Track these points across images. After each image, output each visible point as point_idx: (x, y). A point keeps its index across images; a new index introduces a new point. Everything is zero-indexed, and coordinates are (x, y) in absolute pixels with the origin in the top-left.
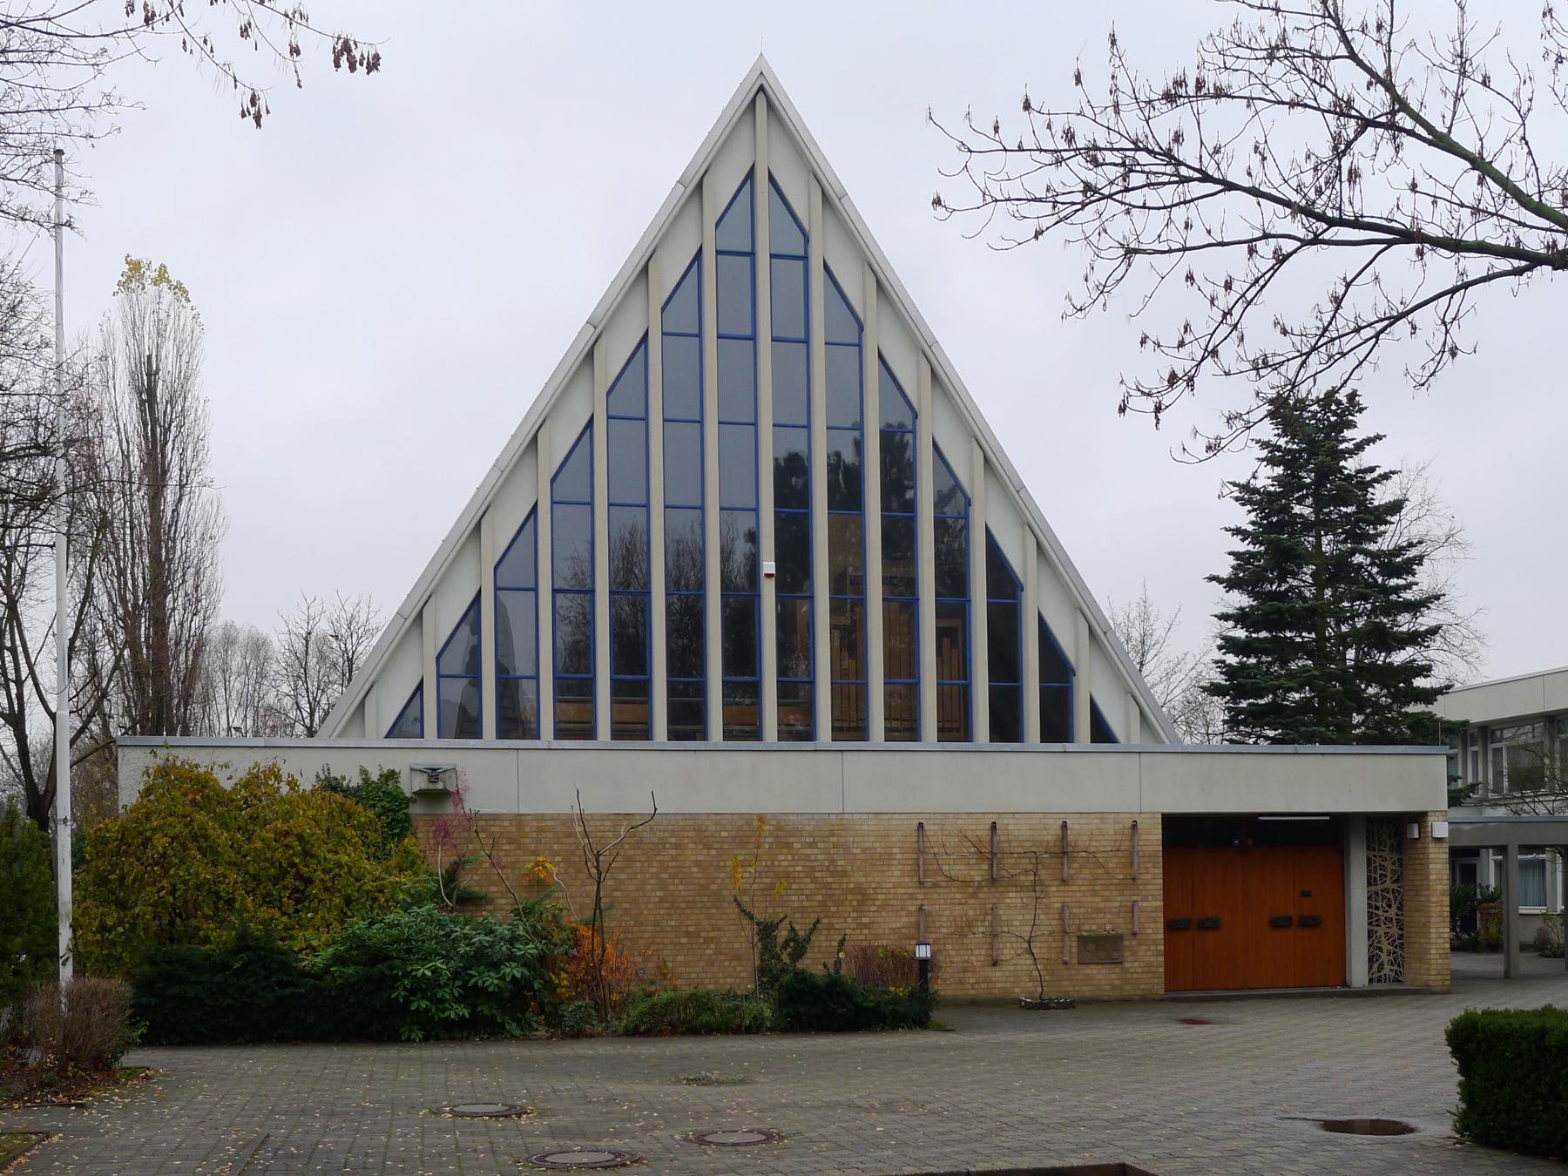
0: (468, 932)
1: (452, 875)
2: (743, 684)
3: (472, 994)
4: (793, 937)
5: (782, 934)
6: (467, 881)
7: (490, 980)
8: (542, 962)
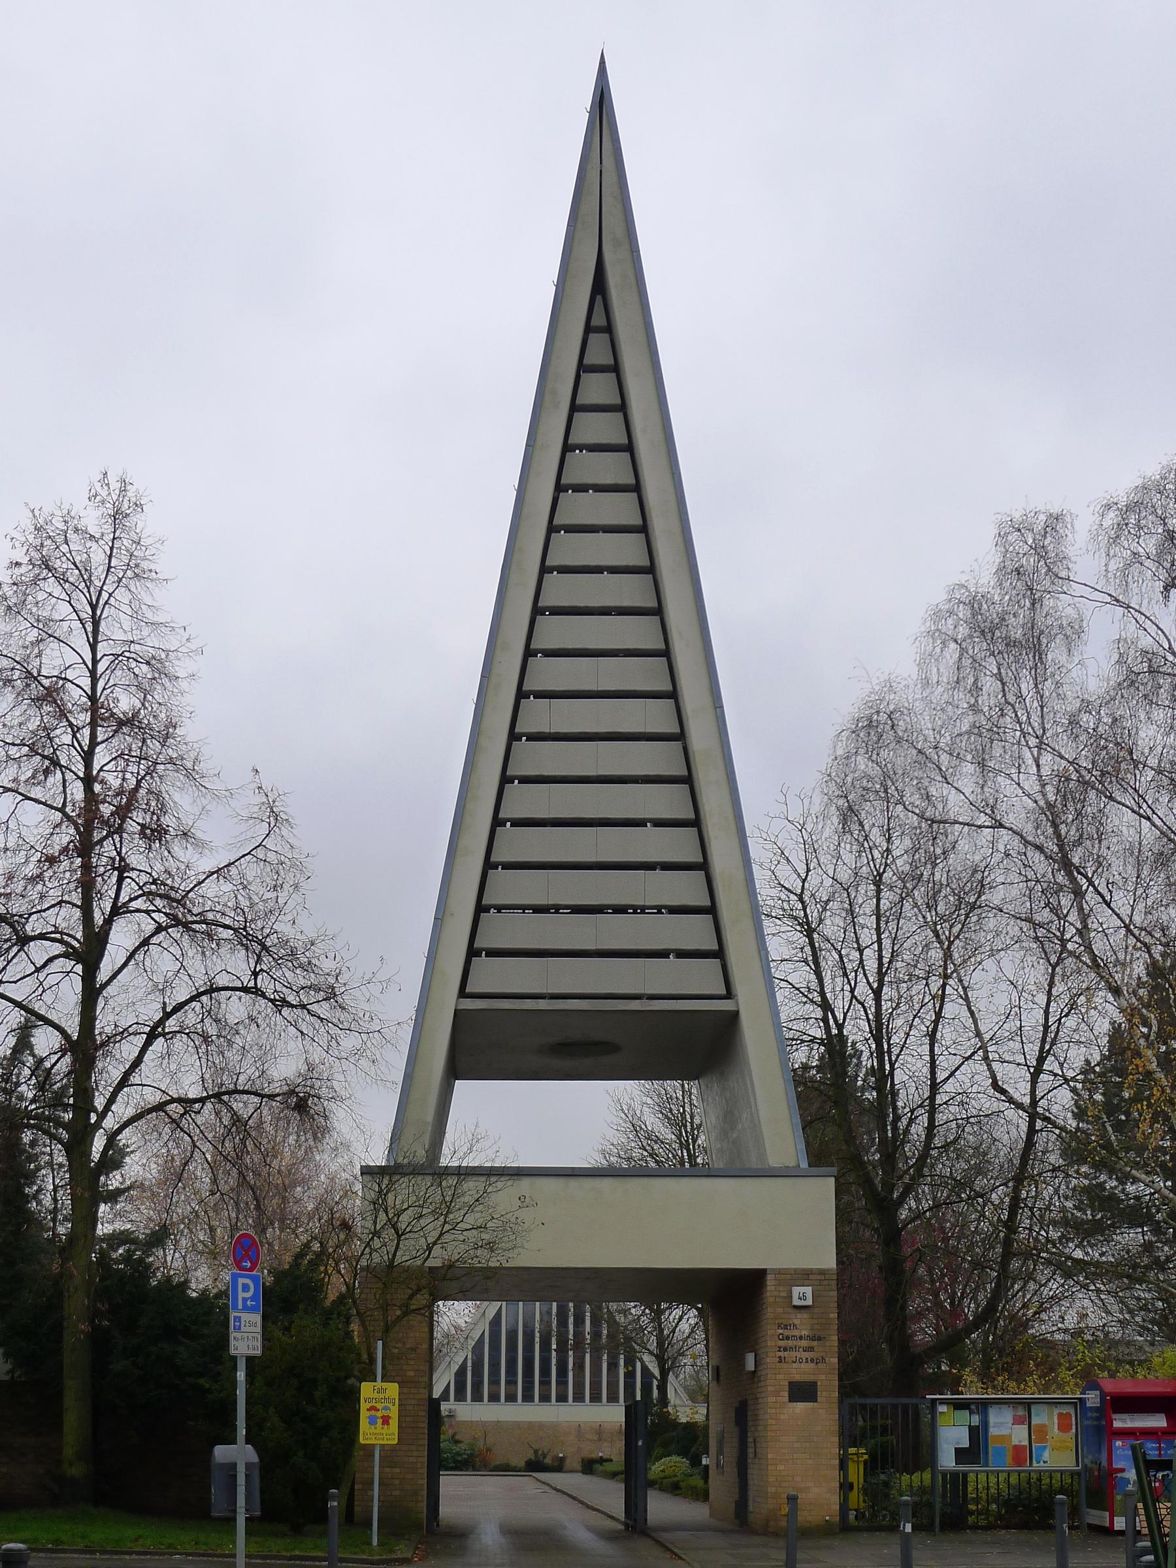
0: (456, 1448)
1: (453, 1436)
2: (545, 1383)
3: (456, 1461)
4: (543, 1453)
5: (540, 1453)
6: (457, 1437)
7: (460, 1458)
8: (471, 1455)
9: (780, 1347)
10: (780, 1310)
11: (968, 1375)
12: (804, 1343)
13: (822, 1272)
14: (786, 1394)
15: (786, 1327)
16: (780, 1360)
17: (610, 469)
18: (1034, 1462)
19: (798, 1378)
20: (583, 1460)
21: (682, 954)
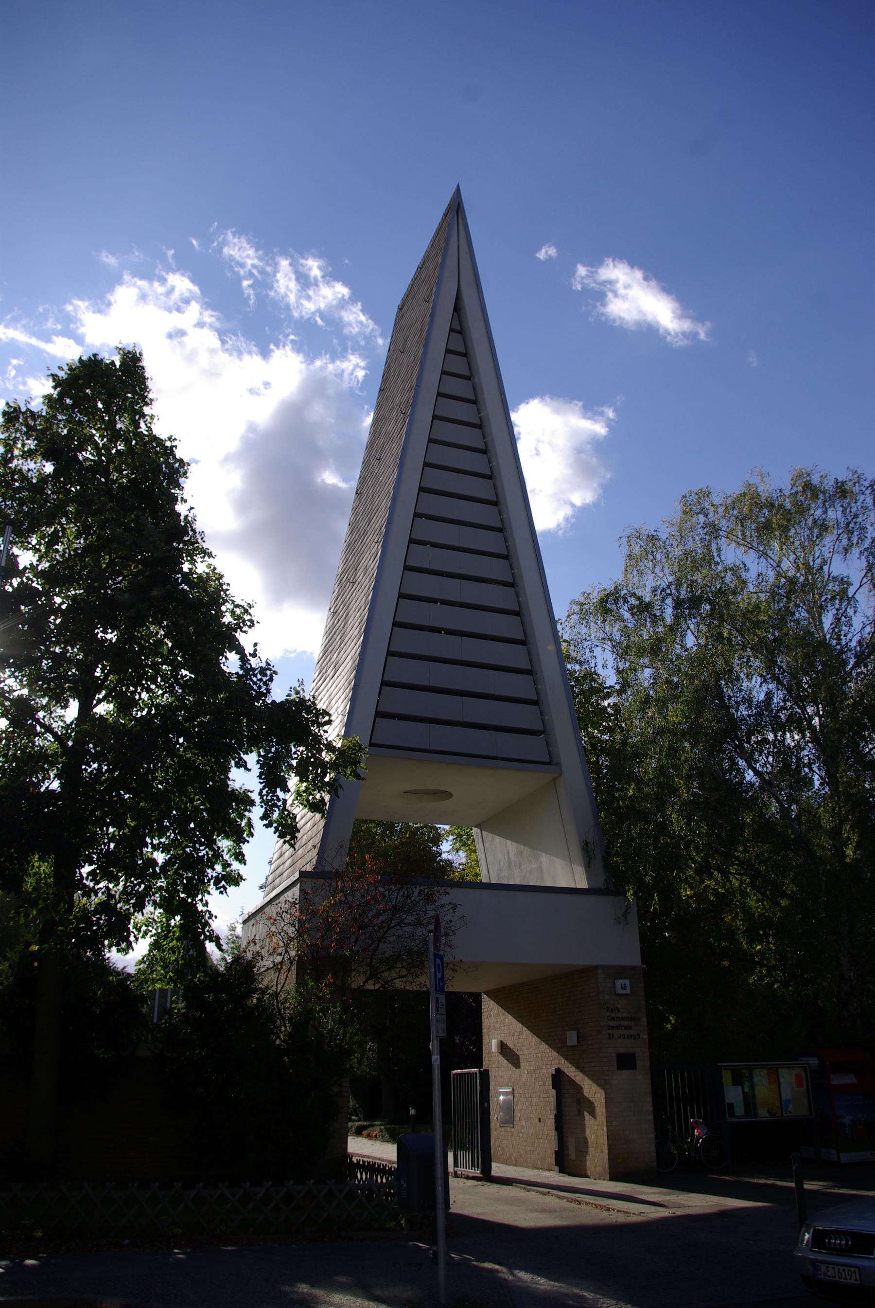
9: (609, 1026)
10: (607, 997)
11: (249, 267)
12: (625, 1023)
13: (633, 968)
14: (615, 1063)
15: (612, 1011)
16: (611, 1036)
17: (462, 411)
18: (784, 1113)
19: (622, 1051)
20: (95, 355)
21: (444, 602)
